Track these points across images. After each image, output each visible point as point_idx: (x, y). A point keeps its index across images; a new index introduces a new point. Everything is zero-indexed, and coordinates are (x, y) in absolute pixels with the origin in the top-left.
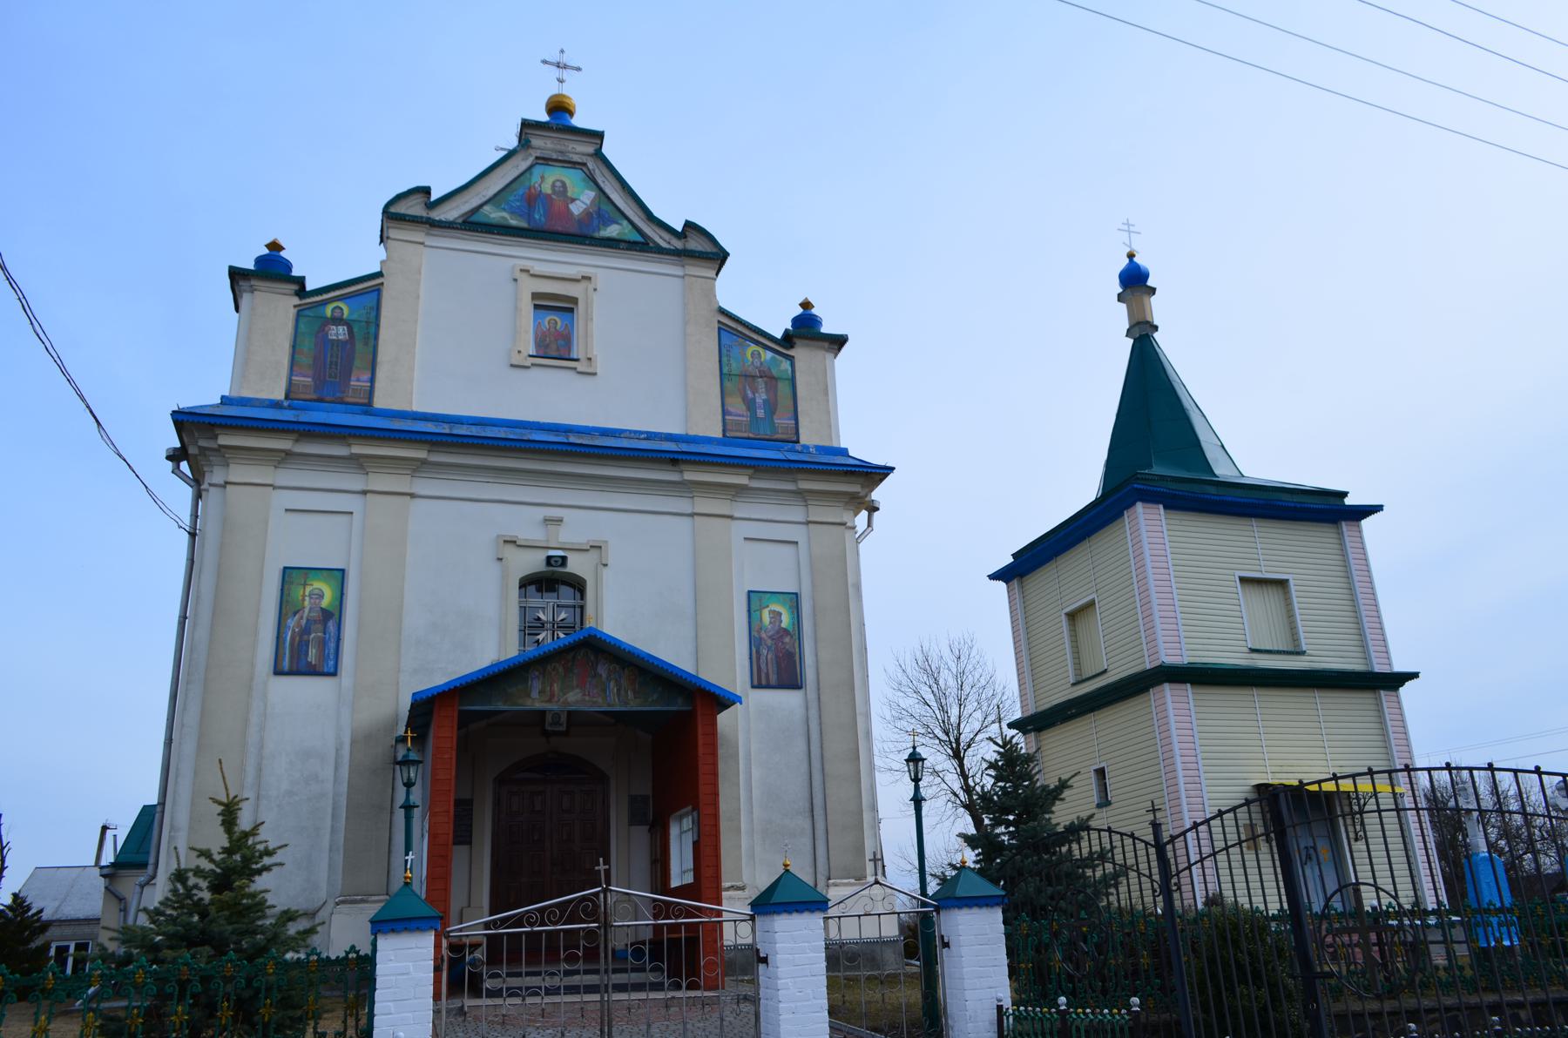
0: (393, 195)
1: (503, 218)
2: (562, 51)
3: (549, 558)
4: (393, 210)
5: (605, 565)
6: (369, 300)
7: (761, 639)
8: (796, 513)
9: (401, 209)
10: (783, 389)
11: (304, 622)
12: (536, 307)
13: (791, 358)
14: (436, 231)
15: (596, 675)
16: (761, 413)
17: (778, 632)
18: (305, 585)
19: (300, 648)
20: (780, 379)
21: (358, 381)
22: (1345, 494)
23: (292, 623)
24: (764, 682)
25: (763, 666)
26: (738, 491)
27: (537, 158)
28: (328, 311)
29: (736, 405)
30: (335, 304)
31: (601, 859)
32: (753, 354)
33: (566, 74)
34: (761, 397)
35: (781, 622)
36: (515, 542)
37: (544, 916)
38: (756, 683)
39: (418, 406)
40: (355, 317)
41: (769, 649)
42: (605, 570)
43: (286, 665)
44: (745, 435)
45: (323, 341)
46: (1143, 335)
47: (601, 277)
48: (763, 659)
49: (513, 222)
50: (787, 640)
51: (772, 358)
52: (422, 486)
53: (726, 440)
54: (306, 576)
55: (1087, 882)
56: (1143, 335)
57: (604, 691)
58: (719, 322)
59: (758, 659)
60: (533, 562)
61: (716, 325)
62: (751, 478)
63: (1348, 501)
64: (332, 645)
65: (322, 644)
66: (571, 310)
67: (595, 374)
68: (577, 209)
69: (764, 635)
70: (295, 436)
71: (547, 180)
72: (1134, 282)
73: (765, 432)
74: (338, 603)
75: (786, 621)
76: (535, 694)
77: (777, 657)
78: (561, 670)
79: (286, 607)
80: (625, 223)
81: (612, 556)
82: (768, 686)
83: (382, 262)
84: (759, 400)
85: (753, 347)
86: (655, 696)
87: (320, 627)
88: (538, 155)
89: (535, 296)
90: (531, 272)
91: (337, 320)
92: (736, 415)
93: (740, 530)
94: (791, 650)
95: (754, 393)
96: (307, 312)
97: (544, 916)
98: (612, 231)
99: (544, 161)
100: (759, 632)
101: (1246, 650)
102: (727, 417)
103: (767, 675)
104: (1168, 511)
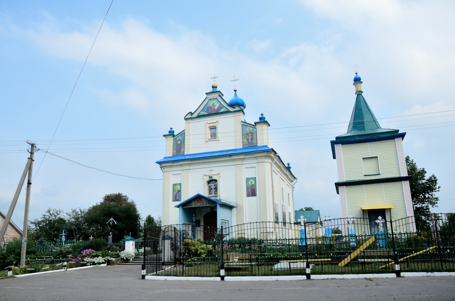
0: (188, 113)
1: (204, 113)
2: (214, 75)
3: (209, 177)
4: (186, 118)
5: (220, 177)
6: (183, 135)
7: (248, 187)
8: (255, 161)
9: (188, 117)
10: (254, 135)
11: (176, 193)
12: (210, 129)
13: (256, 128)
14: (192, 119)
15: (202, 200)
16: (250, 141)
17: (252, 185)
18: (176, 187)
19: (176, 197)
20: (254, 133)
21: (182, 150)
22: (398, 130)
23: (174, 193)
24: (249, 195)
25: (249, 192)
26: (243, 159)
27: (209, 99)
28: (178, 139)
29: (245, 140)
30: (178, 137)
31: (91, 236)
32: (248, 129)
33: (215, 79)
34: (250, 137)
35: (252, 183)
36: (205, 175)
37: (138, 240)
38: (247, 196)
39: (191, 153)
40: (181, 139)
41: (250, 189)
42: (220, 178)
43: (174, 200)
44: (247, 146)
45: (177, 144)
46: (359, 93)
47: (220, 120)
48: (249, 191)
49: (205, 114)
50: (253, 187)
51: (252, 129)
52: (192, 167)
53: (244, 148)
54: (176, 185)
55: (70, 239)
56: (359, 93)
57: (203, 203)
58: (242, 124)
59: (248, 191)
60: (208, 179)
61: (241, 125)
62: (245, 156)
63: (399, 132)
64: (180, 196)
65: (179, 196)
66: (216, 128)
67: (219, 140)
68: (216, 108)
69: (249, 186)
70: (172, 163)
71: (210, 104)
72: (357, 80)
73: (251, 145)
74: (180, 189)
75: (253, 183)
76: (193, 204)
77: (252, 190)
78: (197, 200)
79: (174, 190)
80: (225, 108)
81: (221, 175)
82: (250, 196)
83: (185, 128)
84: (250, 139)
85: (249, 127)
86: (211, 203)
87: (178, 193)
88: (209, 99)
89: (209, 127)
90: (208, 123)
91: (179, 140)
92: (245, 143)
93: (244, 166)
94: (254, 188)
95: (249, 137)
96: (175, 140)
97: (138, 240)
98: (222, 110)
99: (210, 100)
100: (248, 186)
101: (363, 176)
102: (243, 143)
103: (250, 194)
104: (342, 145)
